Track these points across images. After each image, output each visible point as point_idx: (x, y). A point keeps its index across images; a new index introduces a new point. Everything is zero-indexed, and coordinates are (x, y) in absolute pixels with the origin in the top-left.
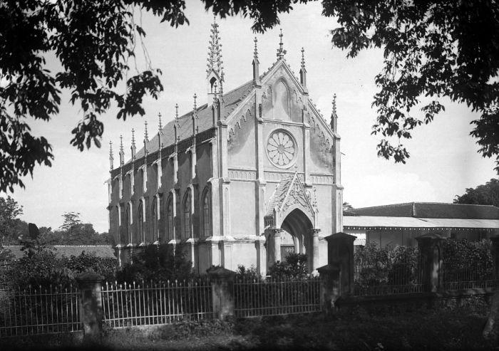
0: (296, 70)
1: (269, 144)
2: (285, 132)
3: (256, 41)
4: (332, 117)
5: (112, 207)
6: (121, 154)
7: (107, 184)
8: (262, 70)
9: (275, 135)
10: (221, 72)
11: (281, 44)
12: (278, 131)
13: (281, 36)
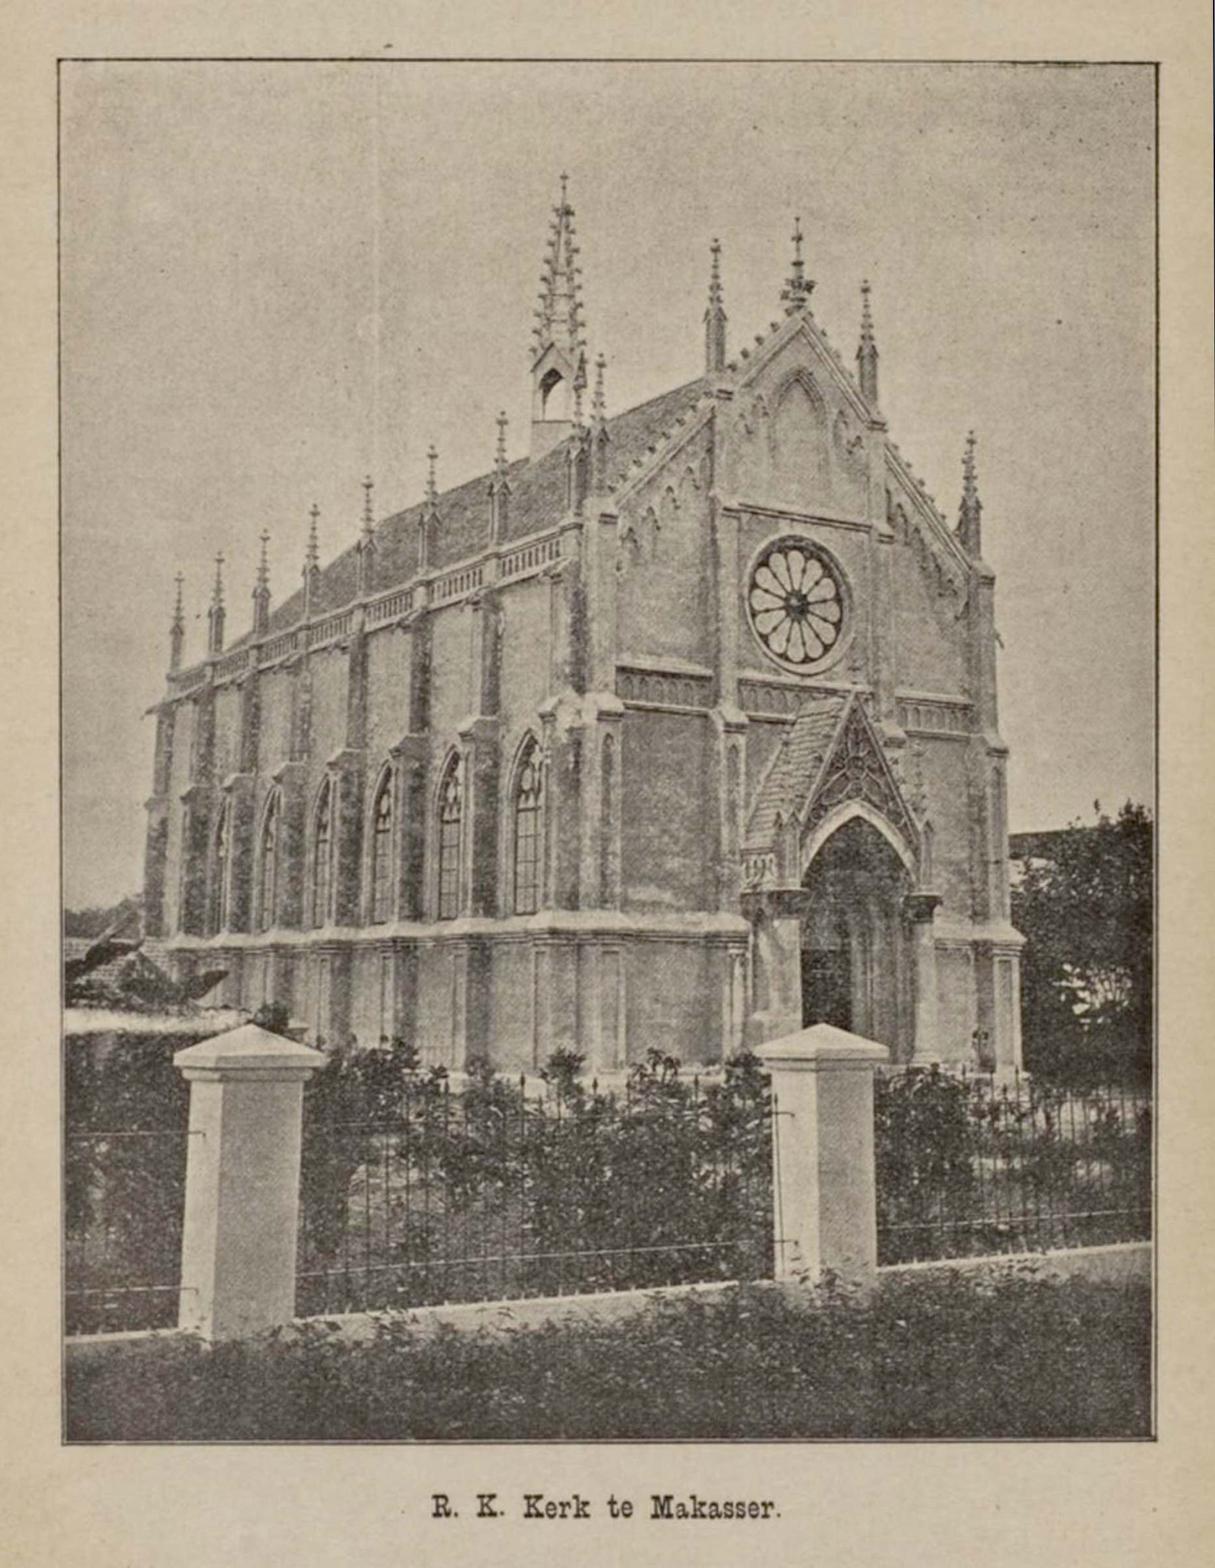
0: (845, 342)
1: (754, 586)
2: (815, 553)
3: (716, 250)
4: (964, 507)
5: (550, 1287)
6: (218, 616)
7: (154, 719)
8: (737, 341)
9: (777, 560)
10: (577, 352)
11: (798, 264)
12: (783, 547)
13: (799, 239)
